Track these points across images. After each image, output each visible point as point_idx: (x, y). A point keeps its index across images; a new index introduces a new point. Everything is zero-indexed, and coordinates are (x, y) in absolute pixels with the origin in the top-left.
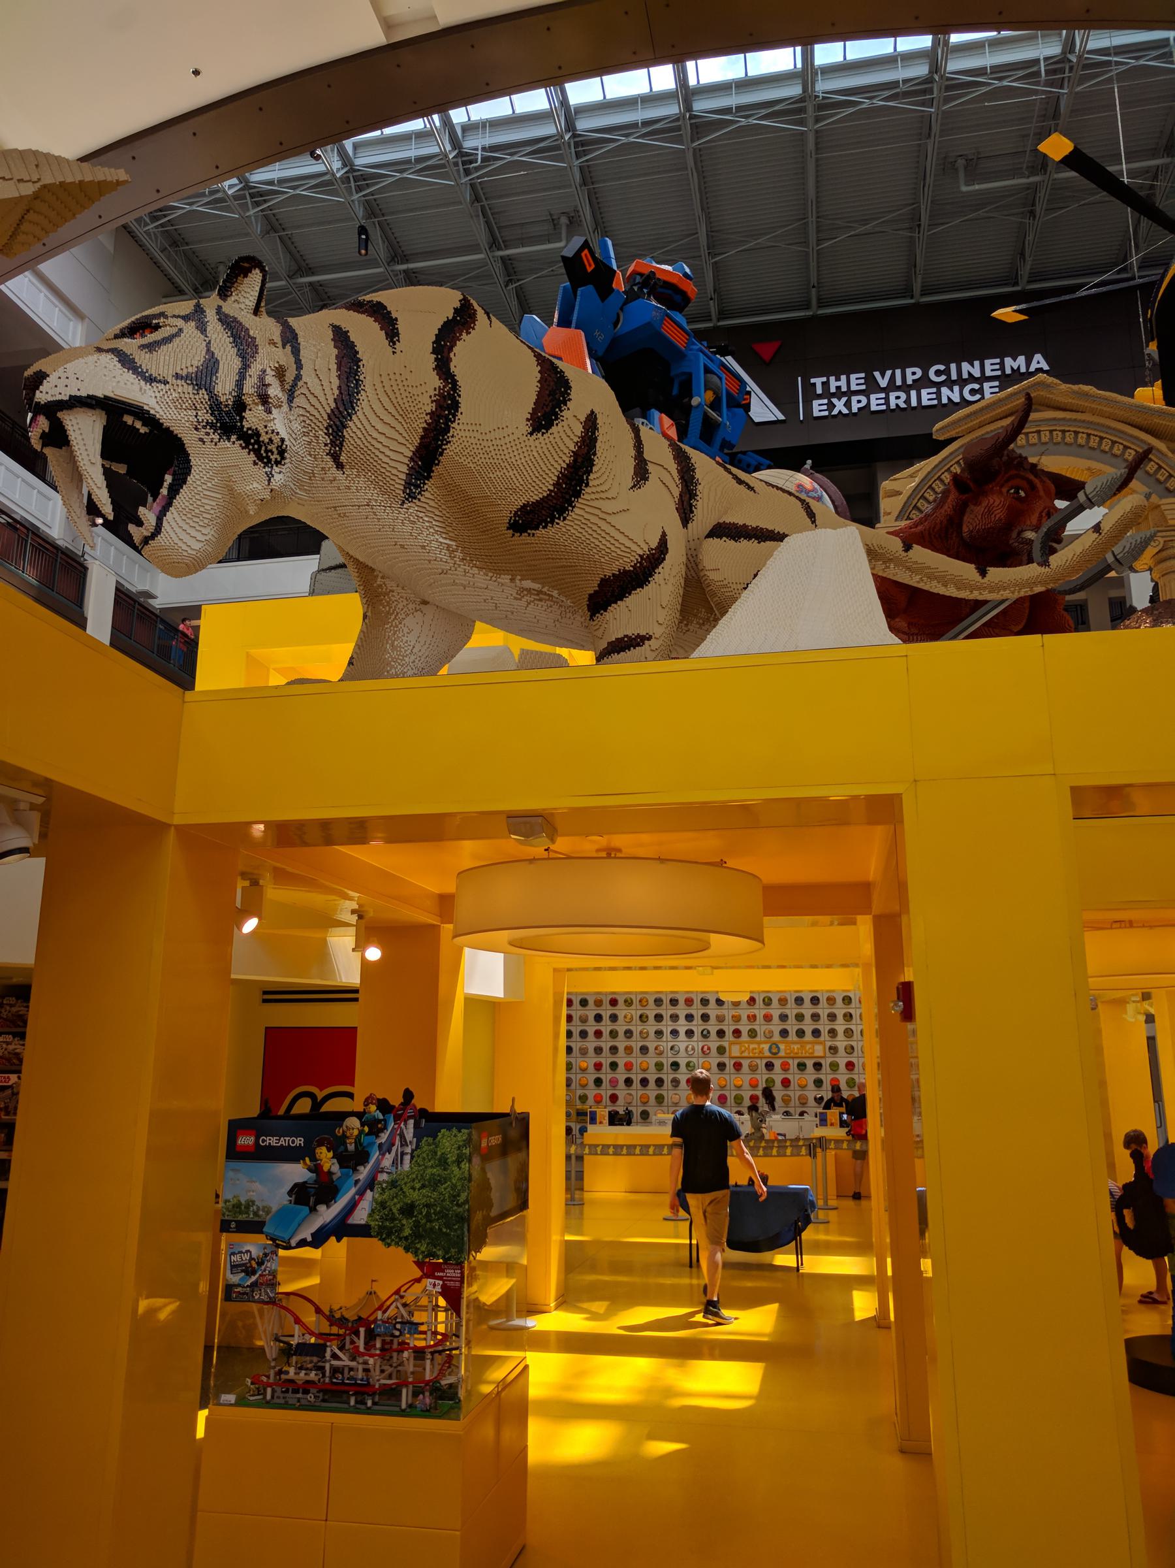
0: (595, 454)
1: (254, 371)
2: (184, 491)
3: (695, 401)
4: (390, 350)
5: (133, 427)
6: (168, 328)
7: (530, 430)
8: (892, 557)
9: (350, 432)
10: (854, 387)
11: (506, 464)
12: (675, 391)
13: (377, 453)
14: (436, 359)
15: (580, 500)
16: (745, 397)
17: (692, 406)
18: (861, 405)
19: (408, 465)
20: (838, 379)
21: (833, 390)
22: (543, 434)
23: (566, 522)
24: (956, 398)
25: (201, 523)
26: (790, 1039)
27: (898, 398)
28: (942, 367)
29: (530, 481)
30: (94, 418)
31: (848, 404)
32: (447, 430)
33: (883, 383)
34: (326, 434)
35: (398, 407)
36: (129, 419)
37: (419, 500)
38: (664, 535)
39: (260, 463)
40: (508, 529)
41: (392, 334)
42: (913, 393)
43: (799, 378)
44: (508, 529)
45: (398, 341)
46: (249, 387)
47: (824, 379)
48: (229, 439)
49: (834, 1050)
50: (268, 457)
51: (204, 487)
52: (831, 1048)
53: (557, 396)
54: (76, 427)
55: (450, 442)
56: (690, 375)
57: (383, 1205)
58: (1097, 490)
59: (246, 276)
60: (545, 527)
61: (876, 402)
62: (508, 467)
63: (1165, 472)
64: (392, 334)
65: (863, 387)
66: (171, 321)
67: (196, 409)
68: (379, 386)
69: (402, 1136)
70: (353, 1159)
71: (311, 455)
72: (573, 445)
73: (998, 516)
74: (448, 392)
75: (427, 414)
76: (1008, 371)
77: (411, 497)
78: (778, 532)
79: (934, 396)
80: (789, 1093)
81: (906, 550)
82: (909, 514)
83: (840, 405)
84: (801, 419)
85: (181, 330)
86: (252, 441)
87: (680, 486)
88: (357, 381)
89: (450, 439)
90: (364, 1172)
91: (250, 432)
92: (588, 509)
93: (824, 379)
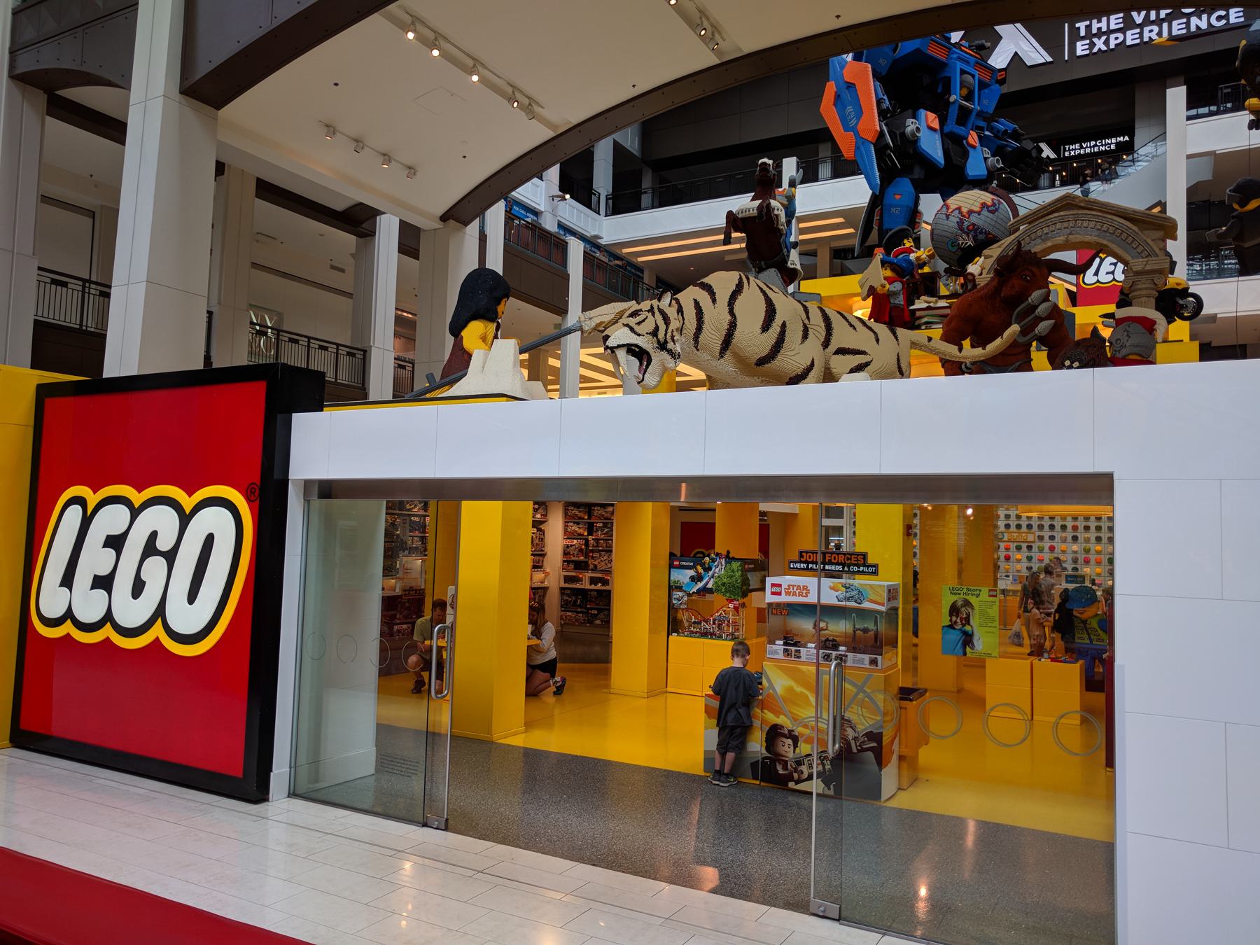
1: (670, 330)
3: (953, 98)
10: (1113, 27)
12: (940, 90)
18: (1118, 41)
24: (1203, 25)
26: (1011, 530)
31: (1107, 43)
32: (733, 334)
36: (633, 348)
38: (813, 359)
41: (714, 301)
42: (1165, 26)
43: (1066, 25)
46: (669, 334)
47: (1088, 23)
49: (1041, 538)
52: (1039, 536)
56: (949, 78)
57: (716, 582)
64: (714, 301)
65: (1121, 25)
66: (644, 313)
69: (721, 564)
70: (708, 569)
77: (722, 357)
80: (1031, 564)
84: (1066, 59)
86: (670, 352)
90: (710, 573)
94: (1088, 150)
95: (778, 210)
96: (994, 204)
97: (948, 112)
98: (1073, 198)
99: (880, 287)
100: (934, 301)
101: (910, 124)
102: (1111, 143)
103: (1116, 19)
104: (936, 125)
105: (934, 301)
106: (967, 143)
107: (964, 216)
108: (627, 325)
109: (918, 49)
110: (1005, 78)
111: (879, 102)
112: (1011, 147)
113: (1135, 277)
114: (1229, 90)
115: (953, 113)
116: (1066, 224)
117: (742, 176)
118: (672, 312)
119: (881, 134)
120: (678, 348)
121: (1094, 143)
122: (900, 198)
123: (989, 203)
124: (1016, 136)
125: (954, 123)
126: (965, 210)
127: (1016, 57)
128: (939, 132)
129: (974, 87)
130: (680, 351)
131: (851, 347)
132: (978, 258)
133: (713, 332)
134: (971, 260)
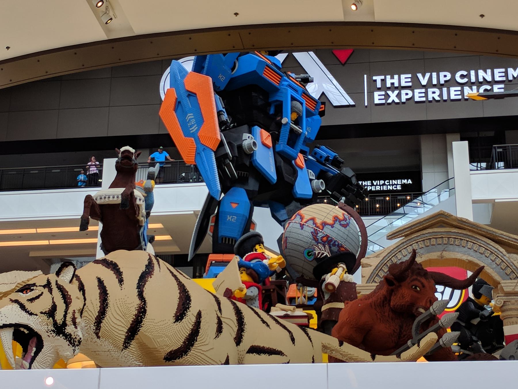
0: (200, 328)
1: (70, 311)
2: (40, 354)
3: (284, 121)
4: (120, 288)
5: (23, 332)
6: (37, 291)
7: (174, 321)
8: (333, 349)
9: (103, 324)
10: (403, 84)
11: (164, 335)
13: (114, 332)
14: (138, 291)
15: (193, 347)
16: (322, 106)
17: (282, 123)
19: (125, 335)
20: (392, 78)
21: (388, 85)
22: (179, 322)
23: (187, 356)
25: (46, 366)
27: (434, 93)
28: (465, 73)
29: (174, 342)
30: (10, 330)
31: (399, 96)
32: (141, 321)
33: (424, 82)
34: (94, 326)
35: (122, 312)
36: (22, 329)
37: (129, 348)
38: (228, 357)
39: (71, 345)
40: (164, 359)
41: (121, 281)
43: (365, 76)
44: (164, 359)
45: (123, 284)
47: (383, 77)
48: (59, 336)
50: (74, 343)
51: (48, 353)
53: (186, 305)
54: (4, 335)
55: (142, 327)
56: (281, 102)
58: (437, 307)
59: (67, 267)
60: (179, 359)
61: (418, 95)
62: (165, 337)
63: (505, 264)
64: (121, 281)
65: (410, 84)
67: (48, 325)
68: (115, 304)
71: (87, 333)
72: (191, 326)
73: (406, 300)
74: (142, 305)
75: (134, 315)
76: (510, 78)
77: (126, 347)
78: (278, 350)
79: (459, 93)
81: (340, 346)
82: (374, 278)
83: (393, 96)
84: (366, 104)
85: (42, 293)
86: (68, 337)
87: (237, 327)
88: (107, 303)
89: (142, 326)
91: (68, 334)
92: (196, 350)
93: (383, 77)
94: (378, 188)
95: (140, 200)
96: (345, 219)
97: (279, 133)
98: (449, 215)
99: (238, 291)
100: (292, 309)
101: (247, 138)
102: (397, 184)
103: (406, 78)
104: (269, 142)
105: (292, 309)
106: (296, 163)
107: (317, 227)
108: (16, 301)
109: (255, 71)
110: (324, 111)
111: (219, 113)
112: (332, 173)
113: (506, 298)
114: (501, 150)
115: (284, 134)
116: (440, 241)
117: (59, 171)
118: (73, 290)
119: (221, 144)
120: (79, 333)
121: (449, 76)
122: (236, 208)
123: (341, 217)
124: (336, 163)
125: (286, 143)
126: (318, 222)
127: (323, 96)
128: (272, 149)
129: (303, 114)
130: (81, 336)
131: (267, 345)
132: (336, 269)
133: (118, 317)
134: (329, 271)
